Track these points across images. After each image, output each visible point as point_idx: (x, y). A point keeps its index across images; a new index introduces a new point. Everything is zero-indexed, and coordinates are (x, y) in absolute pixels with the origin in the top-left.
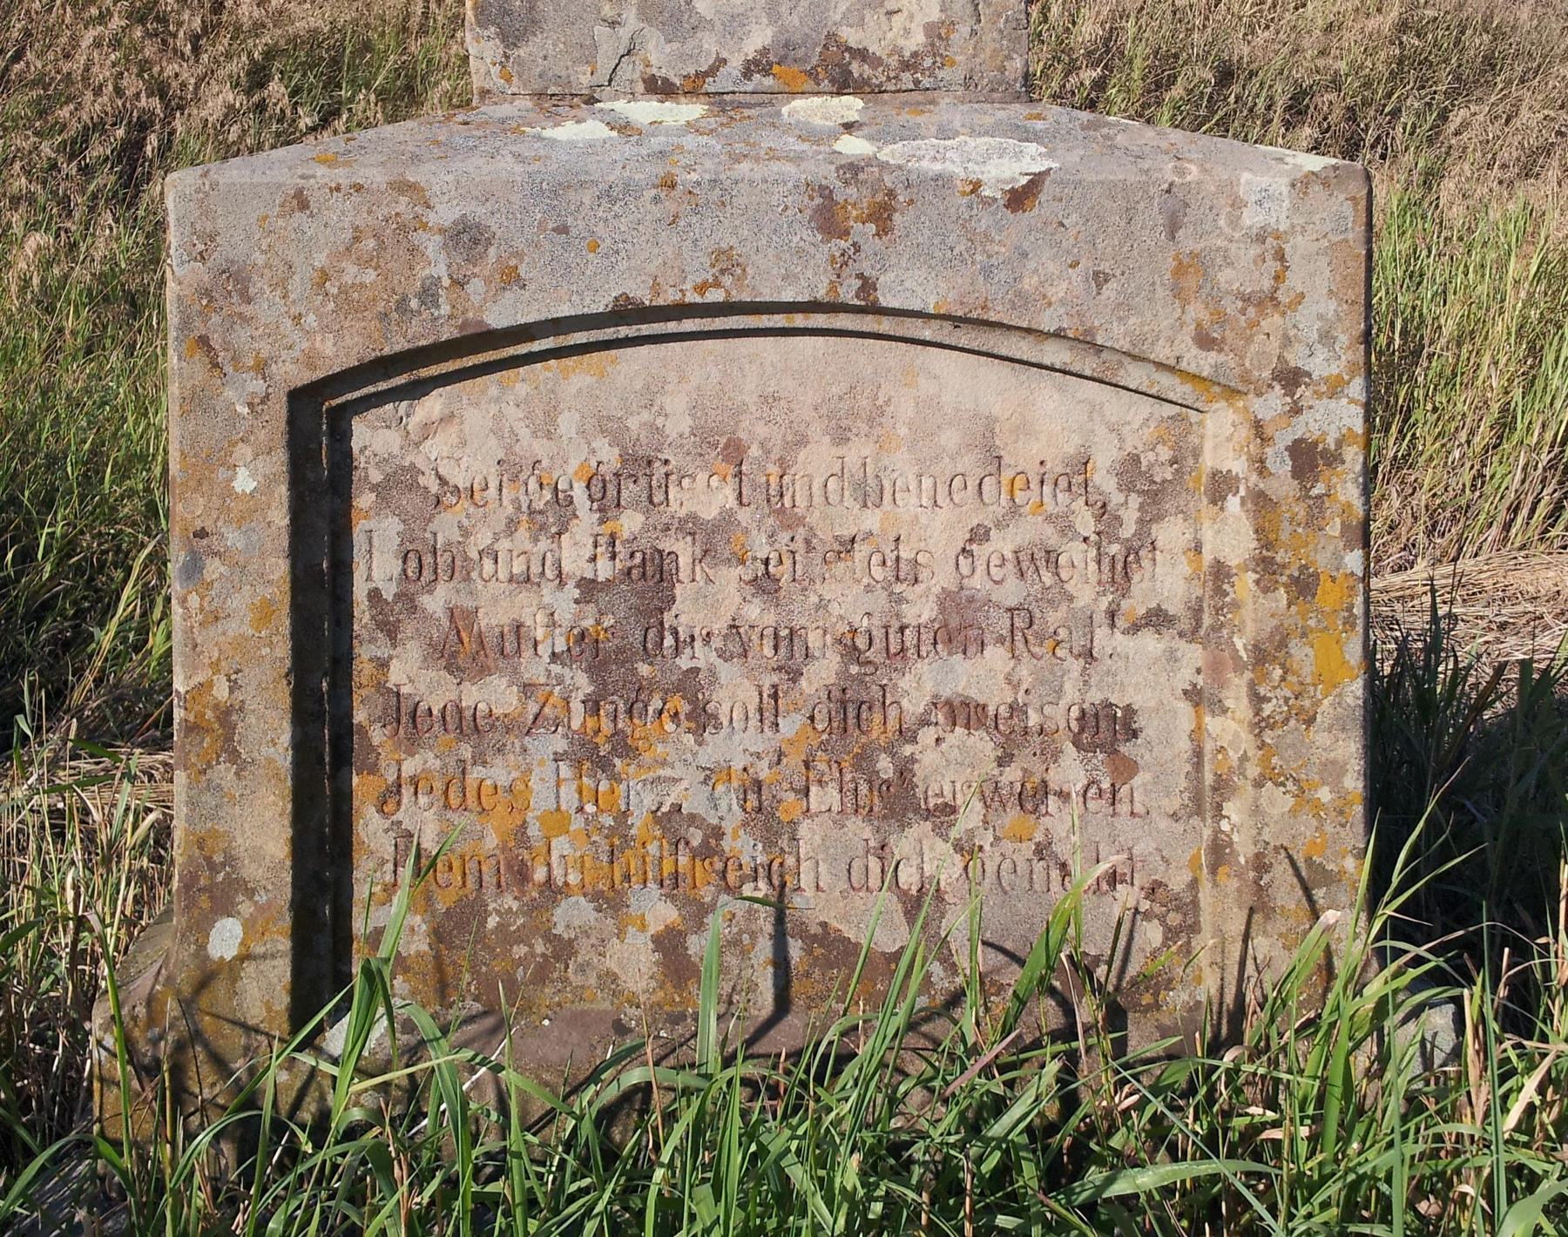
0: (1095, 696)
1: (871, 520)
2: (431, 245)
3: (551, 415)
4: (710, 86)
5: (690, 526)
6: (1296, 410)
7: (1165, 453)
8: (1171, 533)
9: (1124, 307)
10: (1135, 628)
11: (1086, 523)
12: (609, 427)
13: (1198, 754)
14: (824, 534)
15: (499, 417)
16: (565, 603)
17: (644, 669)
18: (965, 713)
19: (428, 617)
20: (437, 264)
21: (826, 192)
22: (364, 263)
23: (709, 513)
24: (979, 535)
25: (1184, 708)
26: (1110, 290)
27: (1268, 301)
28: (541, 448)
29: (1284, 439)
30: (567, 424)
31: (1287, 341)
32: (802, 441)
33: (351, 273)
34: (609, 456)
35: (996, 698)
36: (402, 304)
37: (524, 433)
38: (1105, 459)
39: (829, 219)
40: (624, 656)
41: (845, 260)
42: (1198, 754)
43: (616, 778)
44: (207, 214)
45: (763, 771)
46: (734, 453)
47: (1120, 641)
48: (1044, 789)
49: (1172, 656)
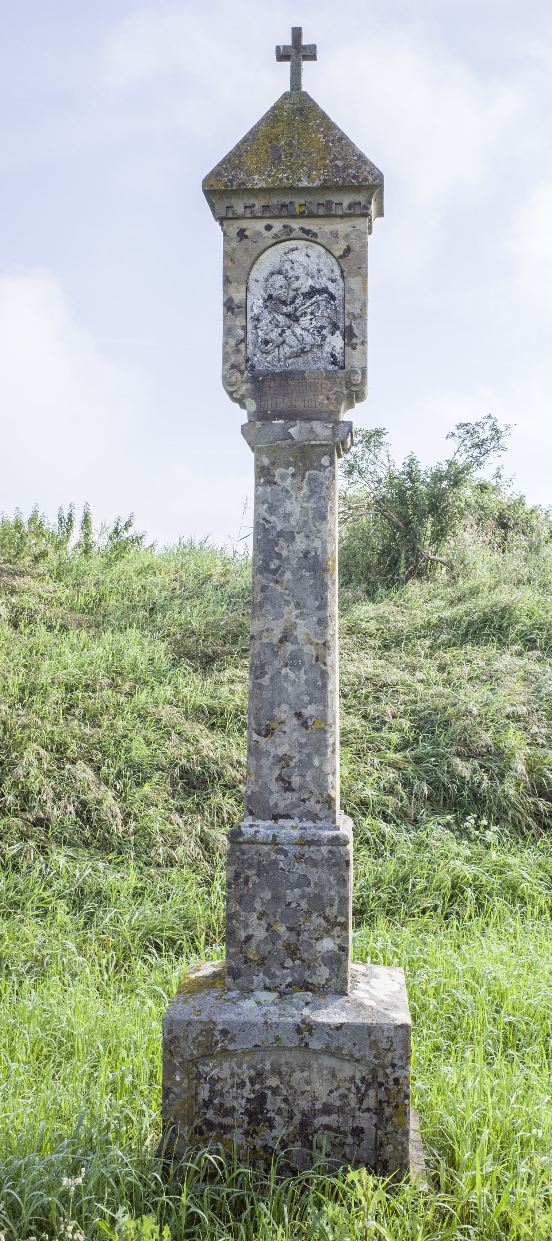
0: (355, 1125)
1: (308, 1088)
2: (217, 1033)
3: (241, 1064)
4: (278, 989)
5: (270, 1088)
6: (395, 1072)
7: (370, 1076)
8: (372, 1093)
9: (359, 1051)
10: (364, 1112)
11: (353, 1090)
12: (253, 1067)
13: (376, 1137)
14: (299, 1090)
15: (230, 1065)
16: (243, 1102)
17: (260, 1116)
18: (327, 1127)
19: (215, 1105)
20: (218, 1037)
21: (298, 1026)
22: (203, 1036)
23: (274, 1085)
24: (331, 1092)
25: (374, 1128)
26: (357, 1047)
27: (389, 1050)
28: (239, 1071)
29: (392, 1077)
30: (244, 1066)
31: (393, 1058)
32: (294, 1071)
33: (201, 1038)
34: (253, 1073)
35: (335, 1125)
36: (211, 1045)
37: (236, 1068)
38: (358, 1077)
39: (299, 1031)
40: (256, 1113)
41: (302, 1039)
42: (376, 1137)
43: (254, 1138)
44: (171, 1025)
45: (285, 1138)
46: (280, 1073)
47: (361, 1114)
48: (344, 1144)
49: (371, 1117)
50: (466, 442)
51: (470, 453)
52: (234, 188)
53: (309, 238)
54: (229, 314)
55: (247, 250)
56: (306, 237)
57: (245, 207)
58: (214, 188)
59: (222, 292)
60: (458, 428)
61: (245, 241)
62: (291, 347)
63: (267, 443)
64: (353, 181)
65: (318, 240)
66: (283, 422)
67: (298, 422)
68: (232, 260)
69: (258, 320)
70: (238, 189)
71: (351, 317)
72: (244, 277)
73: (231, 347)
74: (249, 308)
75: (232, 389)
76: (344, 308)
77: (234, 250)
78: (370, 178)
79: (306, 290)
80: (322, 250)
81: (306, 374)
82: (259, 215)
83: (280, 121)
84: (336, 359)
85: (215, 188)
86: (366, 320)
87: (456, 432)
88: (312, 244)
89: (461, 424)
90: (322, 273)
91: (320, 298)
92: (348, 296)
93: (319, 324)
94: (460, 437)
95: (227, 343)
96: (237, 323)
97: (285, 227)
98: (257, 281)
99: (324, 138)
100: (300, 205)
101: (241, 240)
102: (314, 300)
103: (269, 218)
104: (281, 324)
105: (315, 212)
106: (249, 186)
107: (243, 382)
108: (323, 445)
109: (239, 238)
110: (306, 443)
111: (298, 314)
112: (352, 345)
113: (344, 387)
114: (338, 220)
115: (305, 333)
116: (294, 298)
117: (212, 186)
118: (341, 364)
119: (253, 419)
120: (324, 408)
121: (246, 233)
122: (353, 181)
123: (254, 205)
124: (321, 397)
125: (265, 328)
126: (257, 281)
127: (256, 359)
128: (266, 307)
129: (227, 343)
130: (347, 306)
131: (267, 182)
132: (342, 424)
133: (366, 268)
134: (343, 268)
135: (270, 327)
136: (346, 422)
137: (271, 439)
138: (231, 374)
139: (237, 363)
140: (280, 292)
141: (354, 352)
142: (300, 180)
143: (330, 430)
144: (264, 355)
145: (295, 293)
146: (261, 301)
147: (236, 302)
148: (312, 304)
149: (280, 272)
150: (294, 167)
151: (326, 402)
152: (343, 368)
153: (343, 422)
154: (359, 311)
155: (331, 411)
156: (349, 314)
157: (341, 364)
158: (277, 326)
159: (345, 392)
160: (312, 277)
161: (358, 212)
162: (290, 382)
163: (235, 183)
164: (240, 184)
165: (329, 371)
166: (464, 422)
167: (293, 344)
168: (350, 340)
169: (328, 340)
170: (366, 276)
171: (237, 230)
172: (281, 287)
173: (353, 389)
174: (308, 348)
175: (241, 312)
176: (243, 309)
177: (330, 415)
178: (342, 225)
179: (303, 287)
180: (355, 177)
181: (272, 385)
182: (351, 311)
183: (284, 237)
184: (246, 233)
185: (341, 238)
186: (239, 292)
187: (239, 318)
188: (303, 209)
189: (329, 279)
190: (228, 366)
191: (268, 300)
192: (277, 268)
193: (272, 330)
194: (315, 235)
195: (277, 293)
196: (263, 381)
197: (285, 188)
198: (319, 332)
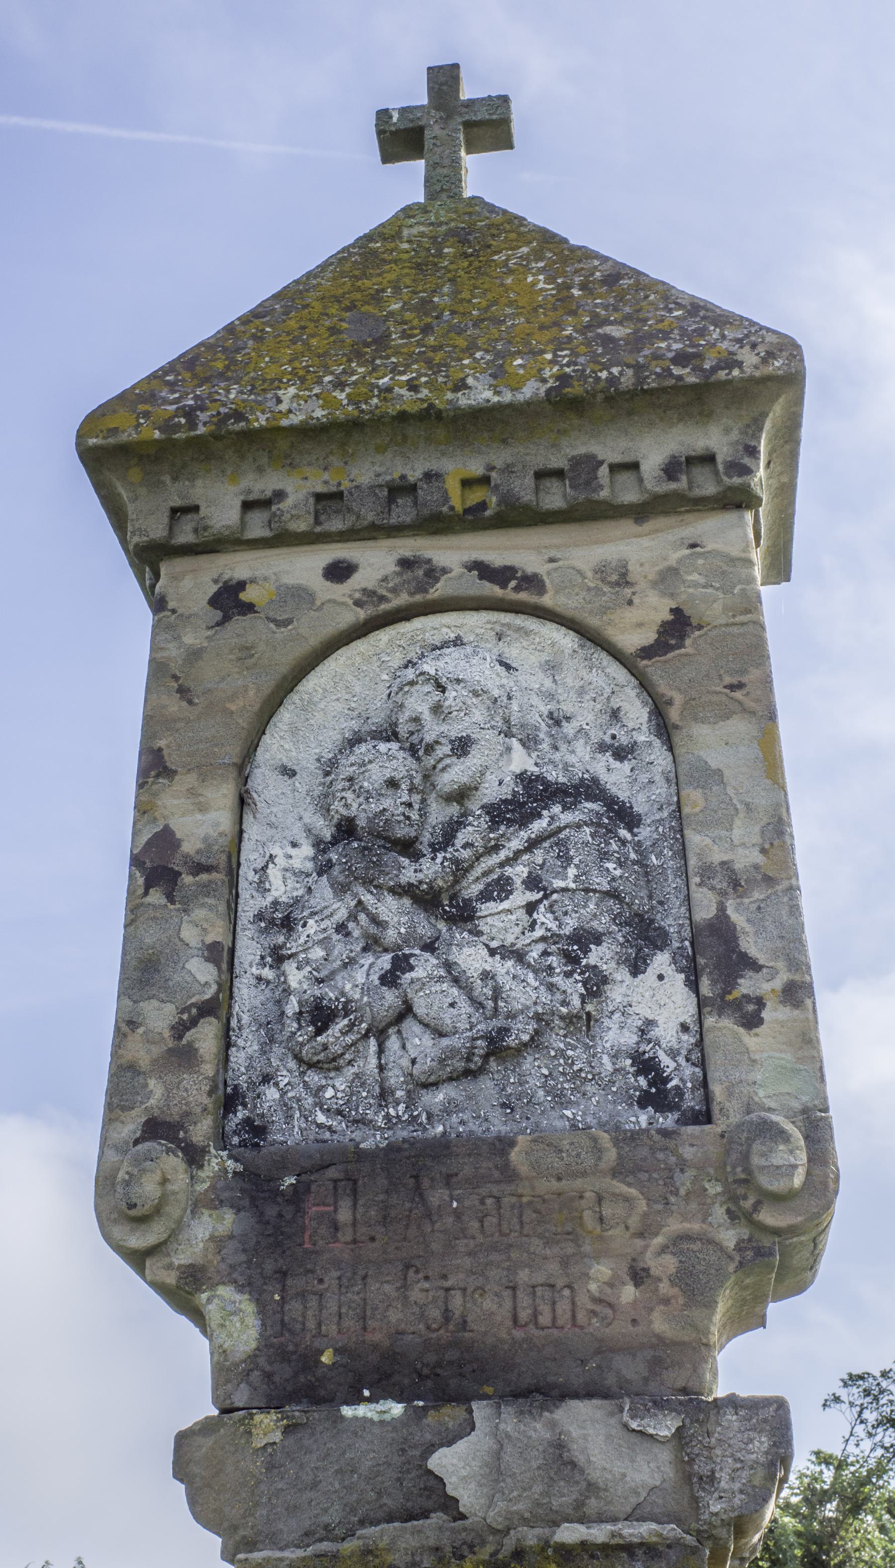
50: (866, 1414)
51: (878, 1438)
52: (201, 430)
53: (509, 594)
54: (156, 897)
55: (246, 652)
56: (494, 590)
57: (247, 506)
58: (124, 438)
59: (130, 814)
60: (846, 1385)
61: (239, 623)
62: (439, 1033)
63: (308, 1536)
64: (677, 371)
65: (547, 600)
66: (397, 1409)
67: (480, 1410)
68: (183, 692)
69: (288, 924)
70: (216, 436)
71: (720, 882)
72: (232, 752)
73: (149, 1039)
74: (247, 874)
75: (137, 1241)
76: (682, 853)
77: (194, 655)
78: (749, 358)
79: (506, 792)
80: (567, 640)
81: (515, 1156)
82: (301, 526)
83: (384, 261)
84: (659, 1079)
85: (128, 435)
86: (793, 890)
87: (843, 1393)
88: (519, 620)
89: (850, 1375)
90: (569, 729)
91: (567, 818)
92: (694, 800)
93: (571, 924)
94: (852, 1404)
95: (132, 1024)
96: (189, 934)
97: (406, 564)
98: (289, 772)
99: (550, 280)
100: (467, 483)
101: (226, 619)
102: (539, 826)
103: (343, 537)
104: (391, 936)
105: (527, 497)
106: (260, 420)
107: (197, 1205)
108: (629, 1549)
109: (218, 615)
110: (531, 1537)
111: (472, 889)
112: (737, 1006)
113: (719, 1213)
114: (627, 526)
115: (504, 968)
116: (450, 831)
117: (114, 431)
118: (691, 1101)
119: (241, 1398)
120: (620, 1329)
121: (249, 595)
122: (677, 371)
123: (280, 495)
124: (602, 1270)
125: (318, 953)
126: (289, 772)
127: (272, 1094)
128: (324, 869)
129: (132, 1024)
130: (695, 839)
131: (328, 403)
132: (730, 1417)
133: (767, 682)
134: (663, 688)
135: (341, 950)
136: (754, 1405)
137: (333, 1516)
138: (137, 1161)
139: (174, 1114)
140: (387, 803)
141: (751, 1040)
142: (461, 386)
143: (665, 1455)
144: (314, 1078)
145: (454, 810)
146: (307, 850)
147: (188, 847)
148: (532, 845)
149: (390, 733)
150: (438, 357)
151: (629, 1293)
152: (704, 1117)
153: (733, 1402)
154: (757, 857)
155: (661, 1341)
156: (707, 872)
157: (691, 1101)
158: (372, 944)
159: (729, 1237)
160: (529, 742)
161: (708, 488)
162: (437, 1196)
163: (203, 416)
164: (223, 420)
165: (634, 1136)
166: (856, 1372)
167: (447, 1018)
168: (728, 978)
169: (616, 994)
170: (772, 716)
171: (214, 589)
172: (393, 784)
173: (768, 1217)
174: (522, 1032)
175: (206, 889)
176: (218, 877)
177: (656, 1365)
178: (645, 542)
179: (491, 779)
180: (681, 359)
181: (344, 1215)
182: (717, 856)
183: (403, 599)
184: (249, 595)
185: (642, 585)
186: (202, 808)
187: (199, 913)
188: (476, 496)
189: (602, 748)
190: (130, 1127)
191: (335, 841)
192: (378, 719)
193: (350, 963)
194: (532, 582)
195: (374, 807)
196: (298, 1195)
197: (403, 416)
198: (571, 959)
